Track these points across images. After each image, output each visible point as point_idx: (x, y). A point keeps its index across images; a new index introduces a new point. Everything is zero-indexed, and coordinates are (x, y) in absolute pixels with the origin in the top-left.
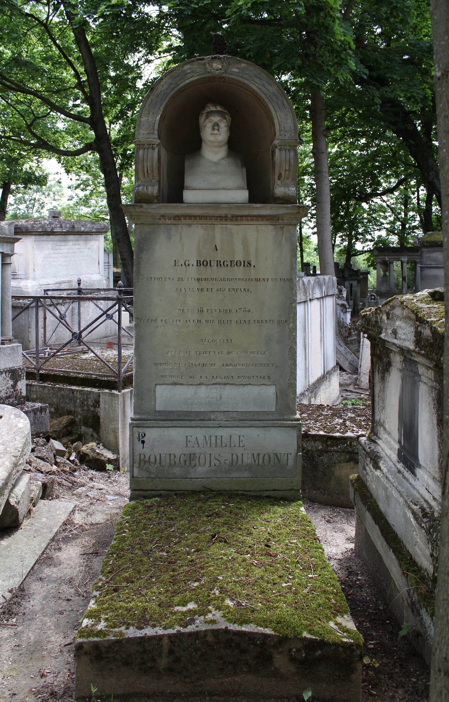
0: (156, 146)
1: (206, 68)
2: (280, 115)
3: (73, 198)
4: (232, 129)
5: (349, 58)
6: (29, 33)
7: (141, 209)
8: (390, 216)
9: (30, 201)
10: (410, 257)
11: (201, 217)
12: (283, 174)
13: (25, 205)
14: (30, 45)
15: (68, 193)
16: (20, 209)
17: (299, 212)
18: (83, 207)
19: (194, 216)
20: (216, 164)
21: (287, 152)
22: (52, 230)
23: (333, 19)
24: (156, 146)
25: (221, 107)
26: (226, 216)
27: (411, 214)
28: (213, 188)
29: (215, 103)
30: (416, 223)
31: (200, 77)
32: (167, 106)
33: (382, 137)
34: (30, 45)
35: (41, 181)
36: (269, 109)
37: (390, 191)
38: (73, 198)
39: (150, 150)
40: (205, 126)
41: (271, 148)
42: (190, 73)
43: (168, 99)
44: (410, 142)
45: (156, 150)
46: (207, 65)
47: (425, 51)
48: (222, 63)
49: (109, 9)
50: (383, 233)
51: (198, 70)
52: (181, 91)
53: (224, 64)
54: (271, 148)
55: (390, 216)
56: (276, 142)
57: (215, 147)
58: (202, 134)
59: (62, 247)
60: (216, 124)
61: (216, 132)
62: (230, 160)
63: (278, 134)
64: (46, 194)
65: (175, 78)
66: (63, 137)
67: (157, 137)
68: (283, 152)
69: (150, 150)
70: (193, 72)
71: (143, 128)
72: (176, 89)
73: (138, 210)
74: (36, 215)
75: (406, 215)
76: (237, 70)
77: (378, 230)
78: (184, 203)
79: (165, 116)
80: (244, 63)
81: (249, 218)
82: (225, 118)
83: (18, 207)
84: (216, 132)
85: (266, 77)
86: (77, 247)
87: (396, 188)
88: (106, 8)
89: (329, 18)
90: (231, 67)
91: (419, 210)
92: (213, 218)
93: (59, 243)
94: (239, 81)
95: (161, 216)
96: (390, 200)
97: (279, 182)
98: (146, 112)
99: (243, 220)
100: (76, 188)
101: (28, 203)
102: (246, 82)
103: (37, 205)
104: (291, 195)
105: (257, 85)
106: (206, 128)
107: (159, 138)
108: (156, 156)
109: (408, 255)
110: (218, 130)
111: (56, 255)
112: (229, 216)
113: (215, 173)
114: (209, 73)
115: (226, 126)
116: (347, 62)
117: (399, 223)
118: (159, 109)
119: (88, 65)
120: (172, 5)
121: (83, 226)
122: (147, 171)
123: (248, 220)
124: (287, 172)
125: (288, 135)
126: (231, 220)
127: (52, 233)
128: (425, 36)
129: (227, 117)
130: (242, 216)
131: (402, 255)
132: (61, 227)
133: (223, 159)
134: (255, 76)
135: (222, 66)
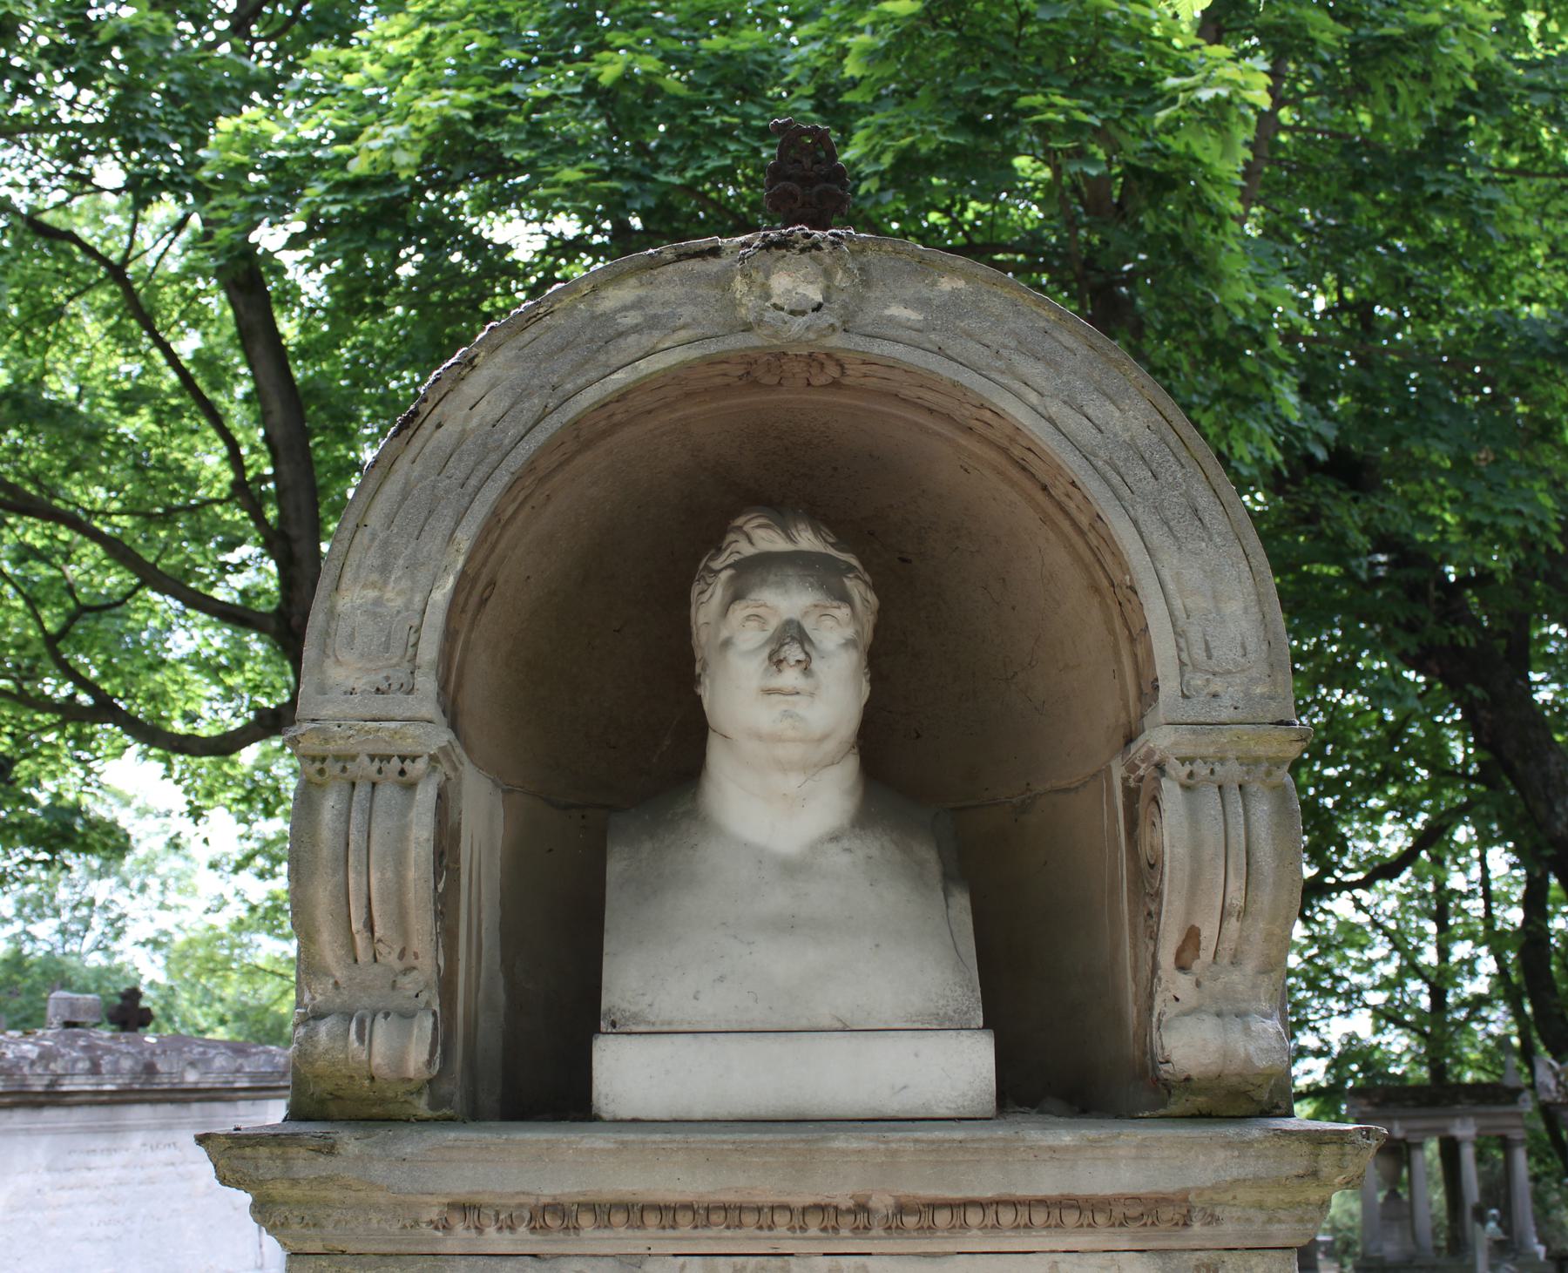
0: (421, 764)
1: (734, 304)
2: (1178, 576)
3: (225, 903)
4: (884, 659)
5: (1275, 373)
6: (72, 307)
7: (324, 1165)
8: (1386, 959)
9: (75, 908)
10: (1485, 1122)
11: (703, 1213)
12: (1208, 933)
13: (54, 923)
14: (76, 349)
15: (210, 884)
16: (33, 939)
17: (1314, 1174)
18: (262, 938)
19: (661, 1209)
20: (792, 869)
21: (1234, 797)
22: (52, 1084)
23: (1213, 221)
24: (421, 764)
25: (817, 532)
26: (862, 1208)
27: (1461, 950)
28: (777, 1021)
29: (780, 510)
30: (1481, 986)
31: (693, 353)
32: (495, 522)
33: (1344, 675)
34: (76, 349)
35: (110, 843)
36: (1109, 541)
37: (1388, 869)
38: (225, 903)
39: (388, 793)
40: (727, 644)
41: (1118, 772)
42: (636, 329)
43: (503, 478)
44: (1470, 694)
45: (426, 795)
46: (739, 285)
47: (1544, 354)
48: (828, 274)
49: (341, 196)
50: (1361, 1024)
51: (687, 312)
52: (585, 435)
53: (840, 278)
54: (1118, 772)
55: (1386, 959)
56: (1160, 739)
57: (784, 767)
58: (705, 692)
59: (98, 1160)
60: (794, 633)
61: (790, 677)
62: (873, 846)
63: (1169, 687)
64: (135, 883)
65: (550, 355)
66: (185, 682)
67: (430, 709)
68: (1210, 801)
69: (388, 793)
70: (653, 323)
71: (345, 656)
72: (554, 422)
73: (304, 1164)
74: (96, 960)
75: (1443, 953)
76: (913, 315)
77: (1341, 1013)
78: (597, 1118)
79: (492, 583)
80: (953, 271)
81: (1007, 1216)
82: (845, 598)
83: (30, 928)
84: (790, 677)
85: (1083, 350)
86: (164, 1155)
87: (1407, 858)
88: (328, 192)
89: (1200, 219)
90: (874, 294)
91: (1494, 939)
92: (781, 1219)
93: (84, 1141)
94: (927, 380)
95: (452, 1206)
96: (1386, 898)
97: (1183, 984)
98: (372, 559)
99: (965, 1226)
100: (238, 867)
101: (66, 915)
102: (967, 378)
103: (98, 923)
104: (1262, 1063)
105: (1033, 398)
106: (733, 657)
107: (452, 714)
108: (421, 830)
109: (1477, 1116)
110: (806, 668)
111: (65, 1196)
112: (882, 1202)
113: (787, 926)
114: (748, 328)
115: (850, 643)
116: (1268, 386)
117: (1414, 985)
118: (451, 538)
119: (277, 415)
120: (581, 175)
121: (192, 1064)
122: (370, 926)
123: (997, 1226)
124: (1233, 925)
125: (1231, 691)
126: (894, 1227)
127: (53, 1098)
128: (1528, 300)
129: (856, 588)
130: (959, 1206)
131: (1454, 1116)
132: (95, 1070)
133: (834, 838)
134: (1025, 349)
135: (827, 292)
